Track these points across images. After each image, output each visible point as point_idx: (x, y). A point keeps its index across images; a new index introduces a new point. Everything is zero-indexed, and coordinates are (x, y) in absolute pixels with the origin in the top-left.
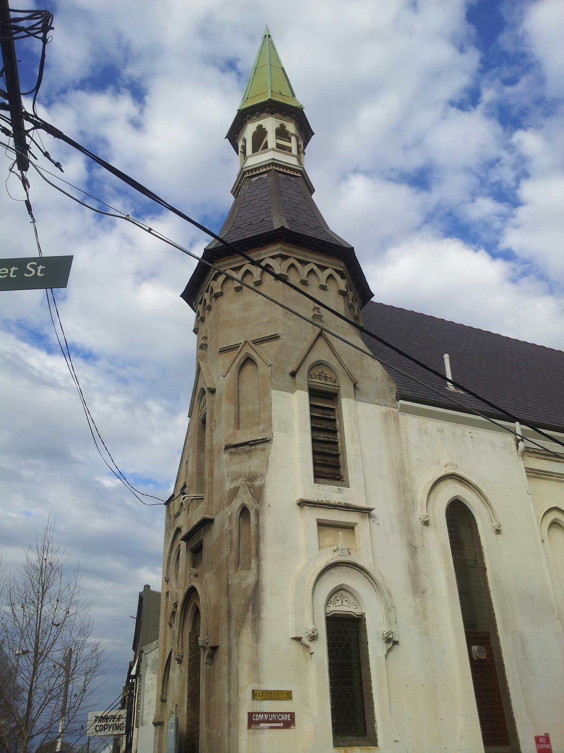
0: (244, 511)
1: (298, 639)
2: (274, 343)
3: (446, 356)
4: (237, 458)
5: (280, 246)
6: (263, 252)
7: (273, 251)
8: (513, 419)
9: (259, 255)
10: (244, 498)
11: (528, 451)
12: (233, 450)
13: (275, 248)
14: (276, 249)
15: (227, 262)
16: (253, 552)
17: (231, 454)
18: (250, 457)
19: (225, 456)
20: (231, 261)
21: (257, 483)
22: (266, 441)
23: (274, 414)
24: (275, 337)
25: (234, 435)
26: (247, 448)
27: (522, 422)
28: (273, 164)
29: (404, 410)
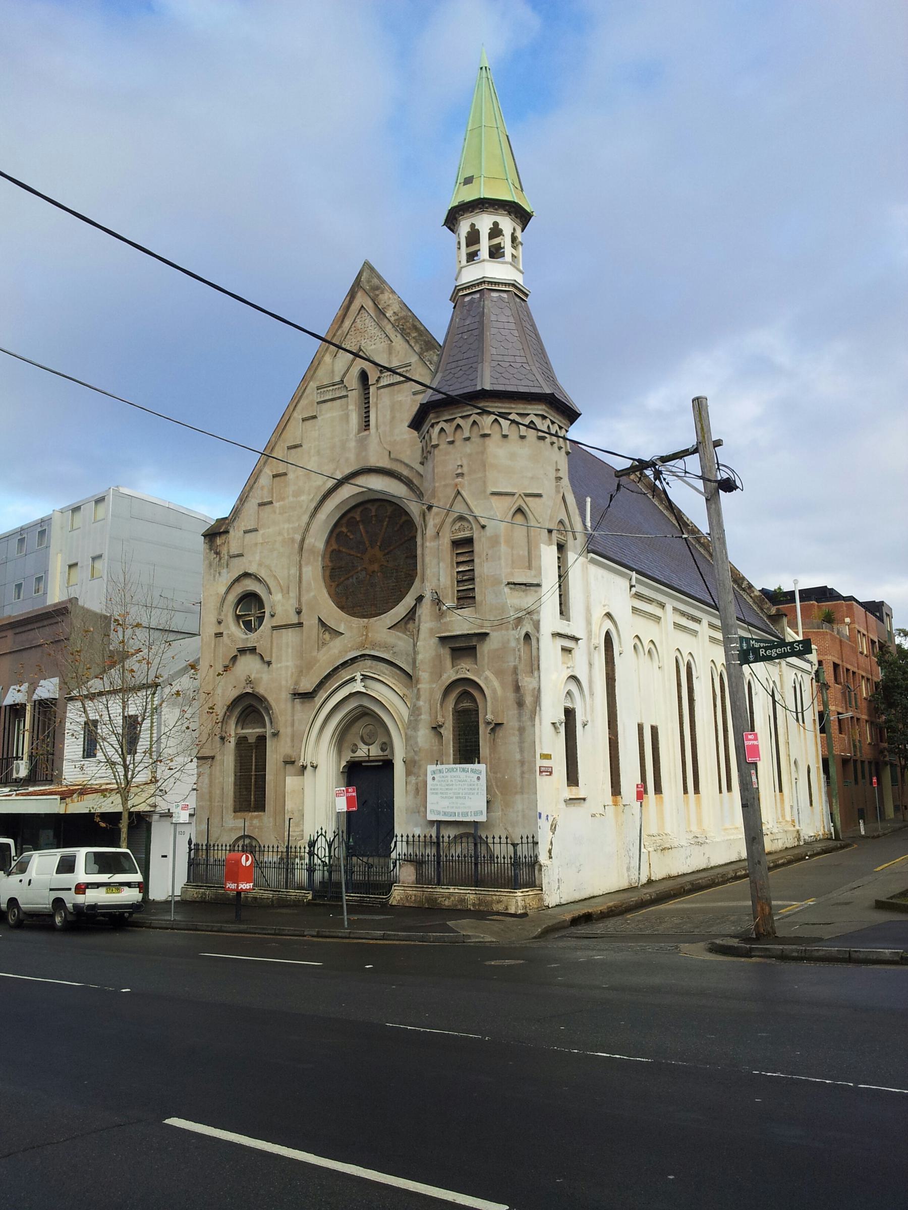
0: (527, 636)
1: (553, 724)
2: (537, 499)
3: (589, 500)
4: (516, 594)
5: (544, 407)
6: (529, 407)
7: (538, 410)
8: (632, 569)
9: (525, 409)
10: (527, 627)
11: (638, 596)
12: (512, 586)
13: (540, 407)
14: (541, 409)
15: (496, 405)
16: (536, 666)
17: (511, 588)
18: (526, 595)
19: (507, 590)
20: (500, 405)
21: (535, 617)
22: (539, 585)
23: (543, 563)
24: (539, 496)
25: (512, 574)
26: (523, 587)
27: (638, 572)
28: (513, 285)
29: (592, 561)
